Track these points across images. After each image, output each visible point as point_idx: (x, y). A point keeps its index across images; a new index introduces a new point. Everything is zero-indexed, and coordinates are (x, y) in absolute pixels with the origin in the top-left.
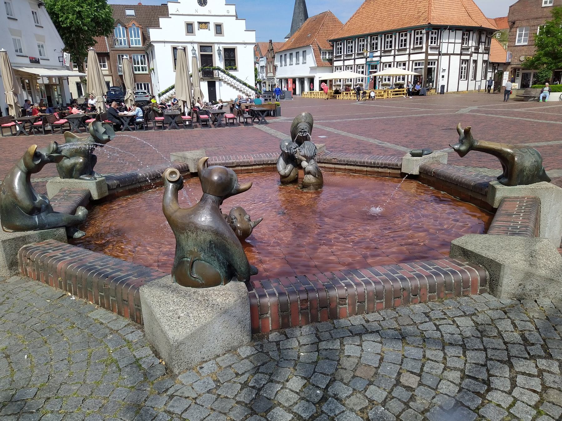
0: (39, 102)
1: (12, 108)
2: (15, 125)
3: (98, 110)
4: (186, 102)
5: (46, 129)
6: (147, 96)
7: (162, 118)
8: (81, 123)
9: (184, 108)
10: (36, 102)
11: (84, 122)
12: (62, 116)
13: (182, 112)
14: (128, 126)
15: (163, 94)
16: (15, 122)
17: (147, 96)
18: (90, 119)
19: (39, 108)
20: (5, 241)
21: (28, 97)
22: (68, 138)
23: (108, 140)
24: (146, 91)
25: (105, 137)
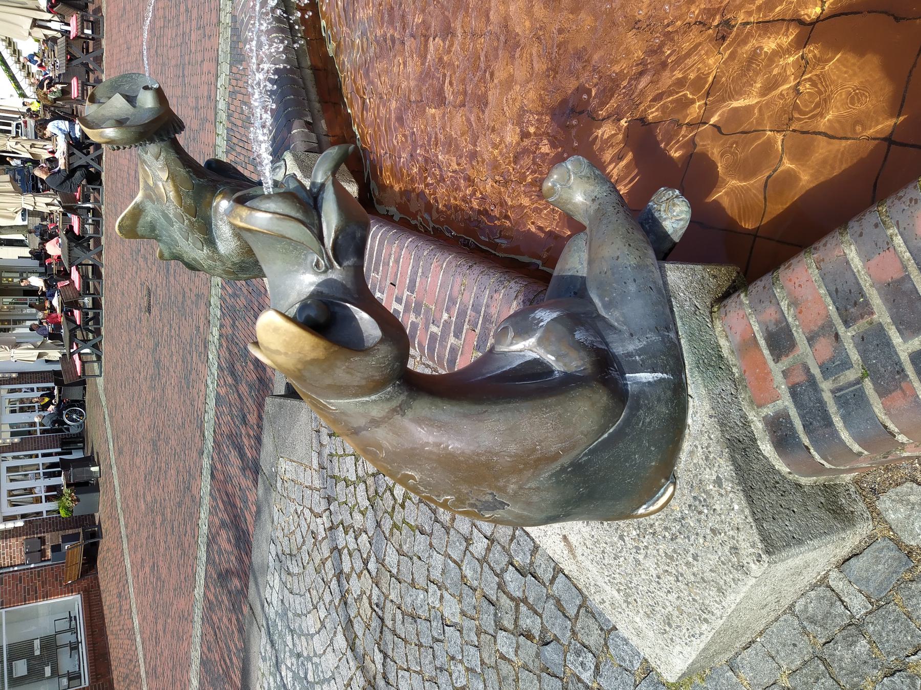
0: (34, 311)
1: (46, 354)
2: (80, 354)
3: (53, 208)
4: (35, 20)
5: (90, 306)
6: (25, 122)
7: (74, 82)
8: (80, 245)
9: (49, 28)
10: (36, 314)
11: (79, 238)
12: (67, 275)
13: (59, 35)
14: (90, 157)
15: (18, 87)
16: (74, 353)
17: (25, 122)
18: (72, 227)
19: (46, 312)
20: (763, 540)
21: (26, 327)
22: (140, 230)
23: (160, 94)
24: (14, 124)
25: (147, 100)
